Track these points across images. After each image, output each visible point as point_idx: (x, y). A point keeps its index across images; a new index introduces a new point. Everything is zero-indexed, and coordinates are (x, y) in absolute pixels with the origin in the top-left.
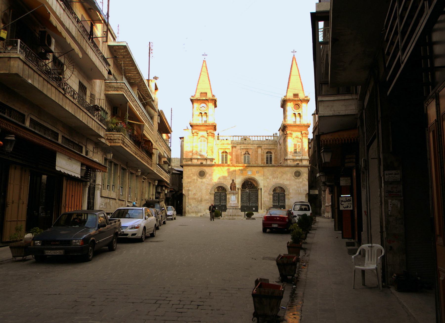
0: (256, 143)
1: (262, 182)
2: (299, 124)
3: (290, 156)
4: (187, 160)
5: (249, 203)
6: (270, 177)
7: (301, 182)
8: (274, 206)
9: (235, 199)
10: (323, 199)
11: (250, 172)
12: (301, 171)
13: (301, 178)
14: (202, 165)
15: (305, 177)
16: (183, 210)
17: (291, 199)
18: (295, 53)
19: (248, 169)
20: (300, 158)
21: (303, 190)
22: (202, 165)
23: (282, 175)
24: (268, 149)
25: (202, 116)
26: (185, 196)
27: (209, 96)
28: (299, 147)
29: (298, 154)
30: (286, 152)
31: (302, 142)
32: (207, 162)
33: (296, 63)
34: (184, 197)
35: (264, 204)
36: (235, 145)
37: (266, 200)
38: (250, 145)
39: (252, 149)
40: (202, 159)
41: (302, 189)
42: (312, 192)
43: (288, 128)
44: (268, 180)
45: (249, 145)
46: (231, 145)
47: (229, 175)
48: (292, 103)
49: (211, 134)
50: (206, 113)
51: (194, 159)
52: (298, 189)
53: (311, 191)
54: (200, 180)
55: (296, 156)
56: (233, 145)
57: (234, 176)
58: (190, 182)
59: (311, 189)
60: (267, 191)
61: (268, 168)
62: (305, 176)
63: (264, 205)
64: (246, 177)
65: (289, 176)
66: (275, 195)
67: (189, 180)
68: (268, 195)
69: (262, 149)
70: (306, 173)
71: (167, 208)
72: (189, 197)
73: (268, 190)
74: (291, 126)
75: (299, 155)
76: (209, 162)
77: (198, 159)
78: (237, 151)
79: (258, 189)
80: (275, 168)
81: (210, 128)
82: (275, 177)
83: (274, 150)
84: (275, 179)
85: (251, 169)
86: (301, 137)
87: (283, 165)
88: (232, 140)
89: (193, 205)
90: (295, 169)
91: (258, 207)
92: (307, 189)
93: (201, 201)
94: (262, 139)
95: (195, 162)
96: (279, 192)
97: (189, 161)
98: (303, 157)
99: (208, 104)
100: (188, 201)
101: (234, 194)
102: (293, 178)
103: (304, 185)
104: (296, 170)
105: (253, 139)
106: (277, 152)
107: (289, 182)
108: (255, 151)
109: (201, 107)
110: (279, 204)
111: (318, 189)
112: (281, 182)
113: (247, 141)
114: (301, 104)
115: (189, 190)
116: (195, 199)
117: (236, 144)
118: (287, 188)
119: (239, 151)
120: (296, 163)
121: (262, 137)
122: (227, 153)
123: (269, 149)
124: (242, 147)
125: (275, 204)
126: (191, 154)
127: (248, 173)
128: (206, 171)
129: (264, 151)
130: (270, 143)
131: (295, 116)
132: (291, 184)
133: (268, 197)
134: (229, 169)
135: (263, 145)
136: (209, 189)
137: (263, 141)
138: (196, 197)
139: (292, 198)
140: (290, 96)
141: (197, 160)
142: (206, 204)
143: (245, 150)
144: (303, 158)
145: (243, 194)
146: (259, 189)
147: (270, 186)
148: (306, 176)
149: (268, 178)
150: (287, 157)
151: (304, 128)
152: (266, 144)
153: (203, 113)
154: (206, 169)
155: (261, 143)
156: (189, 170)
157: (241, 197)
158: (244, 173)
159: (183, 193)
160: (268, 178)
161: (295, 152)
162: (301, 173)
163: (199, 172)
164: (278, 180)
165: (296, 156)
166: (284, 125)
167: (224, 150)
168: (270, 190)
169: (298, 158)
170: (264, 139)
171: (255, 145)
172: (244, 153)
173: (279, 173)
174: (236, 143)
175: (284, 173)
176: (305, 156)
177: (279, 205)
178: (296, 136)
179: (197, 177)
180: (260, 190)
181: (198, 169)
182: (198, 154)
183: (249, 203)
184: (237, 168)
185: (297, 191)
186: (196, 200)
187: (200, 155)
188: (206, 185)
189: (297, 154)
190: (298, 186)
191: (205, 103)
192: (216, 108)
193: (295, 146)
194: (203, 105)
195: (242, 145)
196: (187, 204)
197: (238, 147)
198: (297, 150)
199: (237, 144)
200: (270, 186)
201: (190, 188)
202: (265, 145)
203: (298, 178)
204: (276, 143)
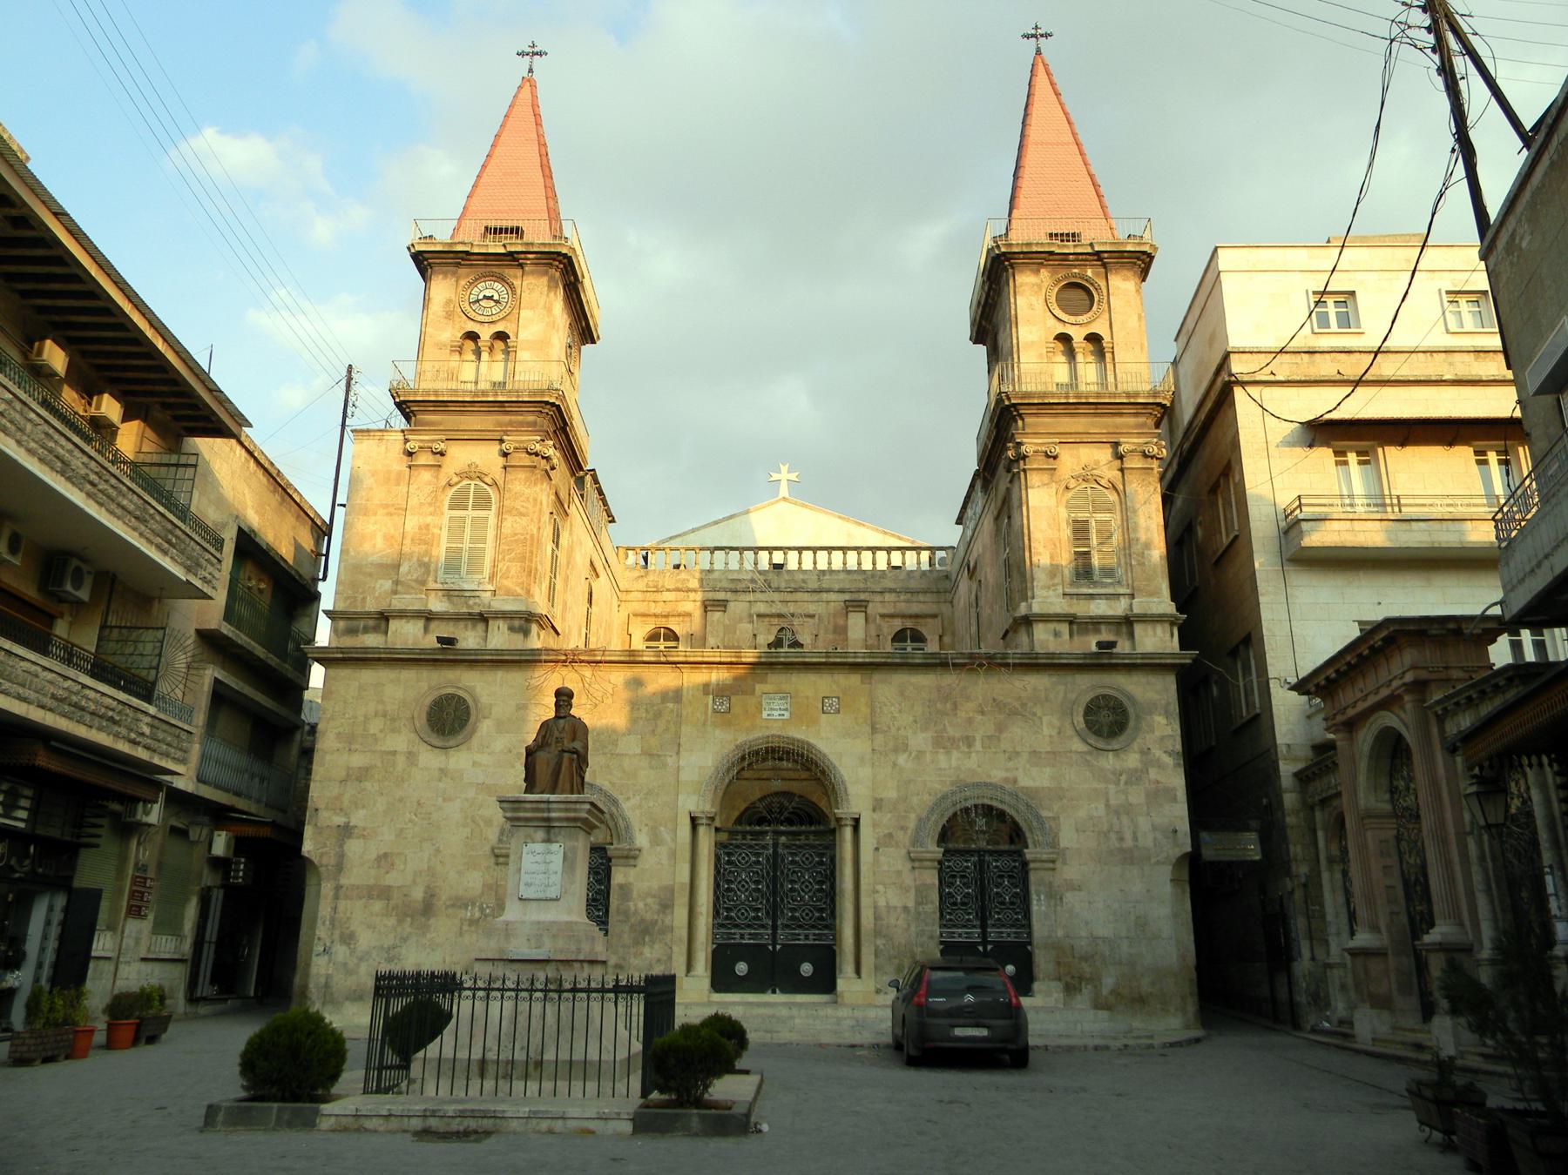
0: (837, 587)
1: (865, 772)
2: (1098, 395)
3: (1046, 598)
4: (355, 623)
5: (774, 928)
6: (920, 740)
7: (1135, 777)
8: (948, 948)
9: (556, 879)
10: (1298, 895)
11: (777, 704)
12: (1130, 697)
13: (1135, 746)
14: (447, 655)
15: (1163, 738)
16: (297, 980)
17: (1069, 897)
18: (1042, 40)
19: (768, 687)
20: (1119, 608)
21: (1154, 828)
22: (447, 655)
23: (1001, 728)
24: (903, 616)
25: (478, 353)
26: (318, 874)
27: (538, 236)
28: (1106, 537)
29: (1105, 585)
30: (1023, 574)
31: (1127, 513)
32: (486, 639)
33: (1053, 84)
34: (311, 881)
35: (877, 933)
36: (721, 596)
37: (888, 907)
38: (806, 596)
39: (812, 616)
40: (456, 618)
41: (1144, 823)
42: (1217, 848)
43: (1028, 420)
44: (902, 759)
45: (799, 596)
46: (699, 596)
47: (634, 721)
48: (1044, 273)
49: (526, 460)
50: (502, 336)
51: (402, 615)
52: (1115, 821)
53: (1204, 835)
54: (430, 759)
55: (1092, 596)
56: (711, 595)
57: (667, 730)
58: (363, 774)
59: (1208, 827)
60: (900, 834)
61: (899, 678)
62: (1157, 733)
63: (880, 942)
64: (751, 737)
65: (1046, 731)
66: (957, 863)
67: (357, 760)
68: (904, 866)
69: (870, 620)
70: (1167, 714)
71: (666, 906)
72: (344, 881)
73: (904, 828)
74: (1045, 406)
75: (1110, 590)
76: (500, 638)
77: (428, 617)
78: (730, 629)
79: (833, 825)
80: (950, 679)
81: (521, 424)
82: (953, 740)
83: (938, 621)
84: (955, 754)
85: (785, 687)
86: (1115, 475)
87: (1005, 656)
88: (708, 567)
89: (365, 940)
90: (1086, 686)
91: (834, 952)
92: (1184, 827)
93: (427, 908)
94: (867, 566)
95: (407, 634)
96: (983, 844)
97: (366, 630)
98: (1139, 606)
99: (517, 283)
100: (335, 909)
101: (549, 828)
102: (1078, 745)
103: (1158, 795)
104: (1093, 687)
105: (823, 565)
106: (953, 634)
107: (1048, 771)
108: (831, 627)
109: (473, 298)
110: (984, 934)
111: (1254, 824)
112: (997, 775)
113: (786, 577)
114: (1102, 284)
115: (346, 831)
116: (384, 893)
117: (725, 590)
118: (1038, 817)
119: (746, 628)
120: (1091, 643)
121: (867, 556)
122: (676, 638)
123: (911, 617)
124: (762, 608)
125: (960, 935)
126: (387, 585)
127: (765, 715)
128: (475, 701)
129: (879, 628)
130: (913, 584)
131: (1071, 353)
132: (1065, 785)
133: (908, 879)
134: (637, 683)
135: (878, 598)
136: (489, 822)
137: (874, 574)
138: (392, 879)
139: (1080, 889)
140: (1029, 233)
141: (421, 623)
142: (461, 935)
143: (775, 621)
144: (1136, 611)
145: (729, 862)
146: (838, 820)
147: (915, 800)
148: (1168, 731)
149: (901, 747)
150: (1030, 607)
151: (1132, 420)
152: (892, 591)
153: (486, 334)
154: (481, 686)
155: (862, 586)
156: (361, 688)
157: (717, 886)
158: (736, 710)
159: (308, 847)
160: (901, 747)
161: (1083, 571)
162: (1131, 711)
163: (428, 701)
164: (972, 763)
165: (1092, 596)
166: (999, 401)
167: (662, 622)
168: (918, 829)
169: (1100, 608)
170: (882, 565)
171: (833, 596)
172: (771, 638)
173: (983, 713)
174: (725, 584)
175: (1014, 713)
176: (1151, 595)
177: (985, 943)
178: (1079, 471)
179: (413, 736)
180: (848, 833)
181: (418, 687)
182: (431, 585)
183: (774, 928)
184: (694, 678)
185: (1113, 836)
186: (388, 899)
187: (449, 593)
188: (471, 793)
189: (1095, 584)
190: (1112, 802)
191: (502, 279)
192: (587, 349)
193: (1075, 531)
194: (495, 289)
195: (759, 596)
196: (322, 931)
197: (738, 607)
198: (1096, 561)
199: (735, 591)
200: (915, 800)
201: (358, 818)
202: (888, 597)
203: (1115, 744)
204: (948, 585)
